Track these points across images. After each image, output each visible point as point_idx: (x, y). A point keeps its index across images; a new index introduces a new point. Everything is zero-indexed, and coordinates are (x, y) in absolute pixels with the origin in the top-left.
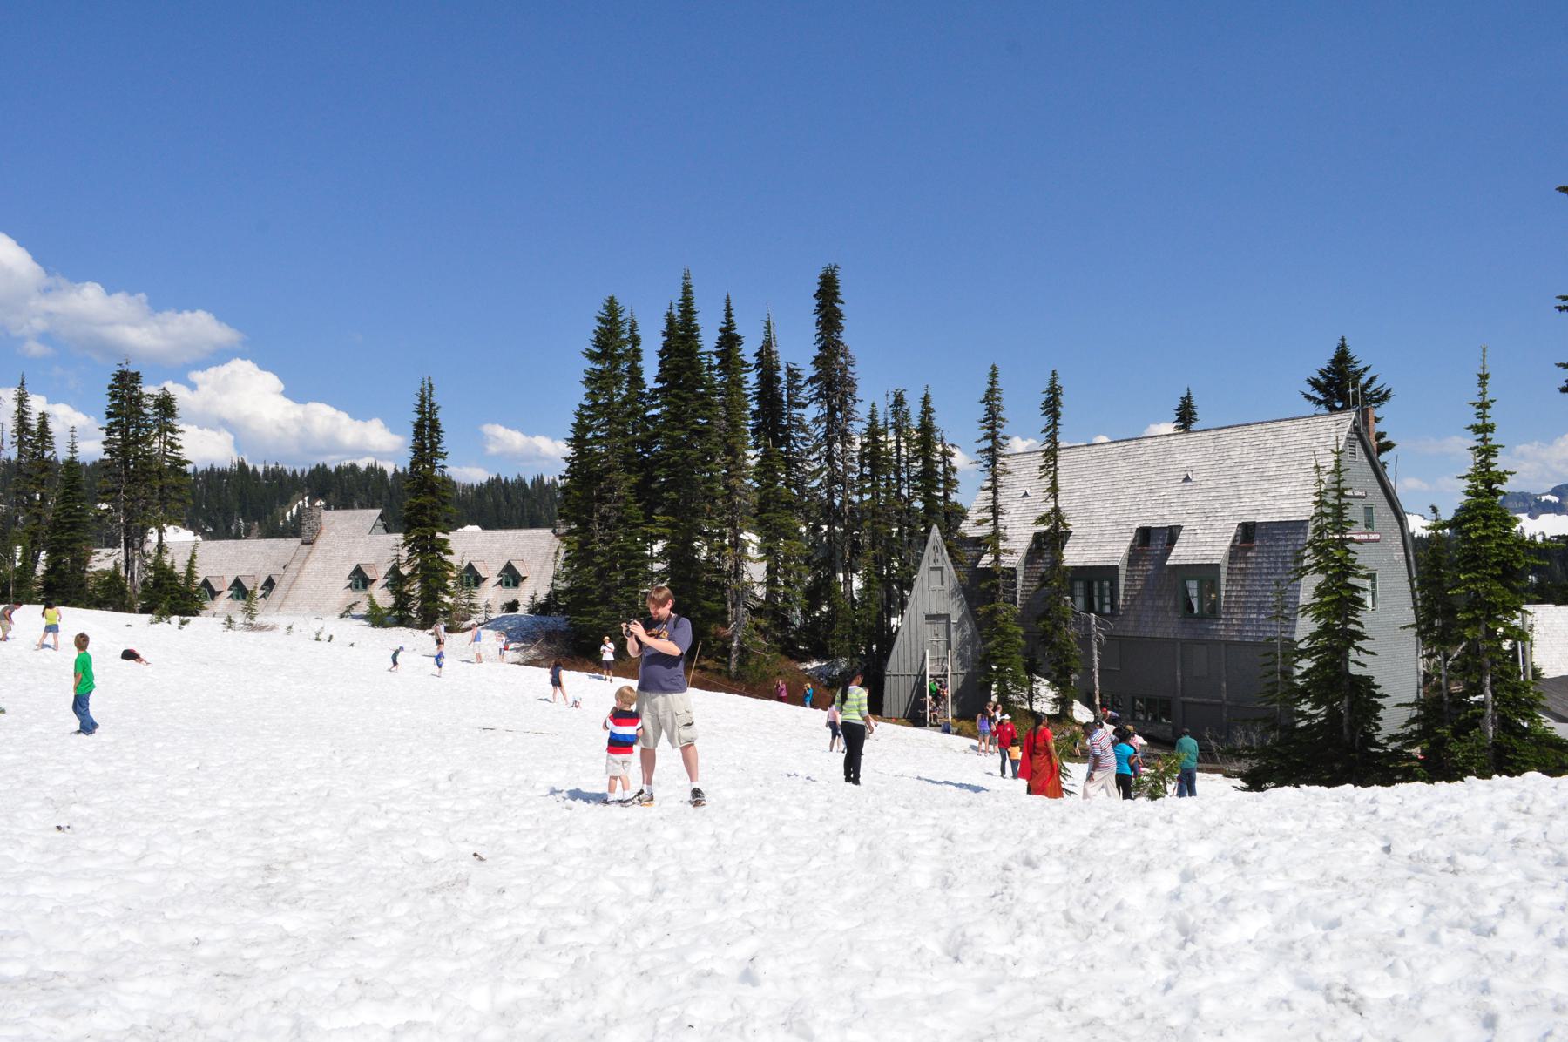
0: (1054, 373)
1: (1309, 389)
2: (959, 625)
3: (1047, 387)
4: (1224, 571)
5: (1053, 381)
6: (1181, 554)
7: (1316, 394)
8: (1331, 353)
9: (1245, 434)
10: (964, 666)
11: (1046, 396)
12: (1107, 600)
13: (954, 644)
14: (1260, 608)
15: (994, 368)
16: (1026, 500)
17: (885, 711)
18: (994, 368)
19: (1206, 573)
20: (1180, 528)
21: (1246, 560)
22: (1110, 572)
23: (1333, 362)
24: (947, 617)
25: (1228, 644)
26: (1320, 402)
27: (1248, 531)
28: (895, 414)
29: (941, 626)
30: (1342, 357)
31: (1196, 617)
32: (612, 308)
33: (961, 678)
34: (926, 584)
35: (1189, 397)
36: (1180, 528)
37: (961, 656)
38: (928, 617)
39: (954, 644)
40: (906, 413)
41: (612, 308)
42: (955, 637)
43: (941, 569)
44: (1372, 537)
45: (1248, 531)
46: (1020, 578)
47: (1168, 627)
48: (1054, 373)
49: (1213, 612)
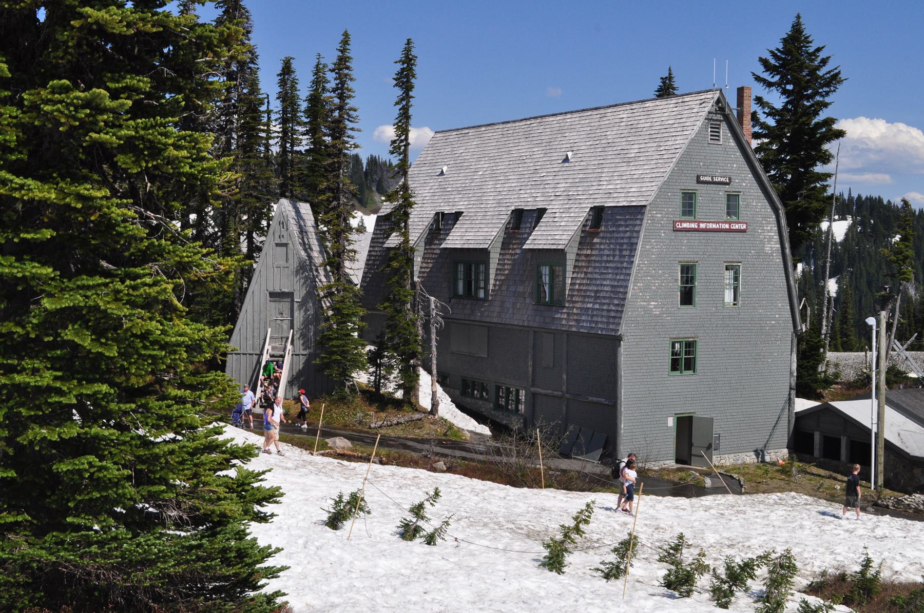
0: (409, 42)
1: (760, 70)
2: (303, 304)
3: (399, 56)
4: (571, 258)
5: (407, 51)
6: (539, 238)
7: (767, 76)
8: (786, 30)
9: (623, 113)
10: (306, 346)
11: (399, 67)
12: (482, 284)
13: (297, 324)
14: (596, 298)
15: (346, 35)
16: (441, 179)
17: (644, 424)
18: (346, 35)
19: (555, 256)
20: (545, 210)
21: (592, 246)
22: (482, 255)
23: (785, 41)
24: (290, 295)
25: (570, 334)
26: (770, 85)
27: (598, 213)
28: (283, 83)
29: (285, 306)
30: (796, 39)
31: (546, 304)
32: (797, 29)
33: (302, 359)
34: (270, 261)
35: (670, 78)
36: (545, 210)
37: (303, 336)
38: (273, 295)
39: (297, 324)
40: (294, 82)
41: (797, 29)
42: (299, 316)
43: (286, 245)
44: (736, 227)
45: (598, 213)
46: (418, 259)
47: (521, 314)
48: (409, 42)
49: (557, 303)
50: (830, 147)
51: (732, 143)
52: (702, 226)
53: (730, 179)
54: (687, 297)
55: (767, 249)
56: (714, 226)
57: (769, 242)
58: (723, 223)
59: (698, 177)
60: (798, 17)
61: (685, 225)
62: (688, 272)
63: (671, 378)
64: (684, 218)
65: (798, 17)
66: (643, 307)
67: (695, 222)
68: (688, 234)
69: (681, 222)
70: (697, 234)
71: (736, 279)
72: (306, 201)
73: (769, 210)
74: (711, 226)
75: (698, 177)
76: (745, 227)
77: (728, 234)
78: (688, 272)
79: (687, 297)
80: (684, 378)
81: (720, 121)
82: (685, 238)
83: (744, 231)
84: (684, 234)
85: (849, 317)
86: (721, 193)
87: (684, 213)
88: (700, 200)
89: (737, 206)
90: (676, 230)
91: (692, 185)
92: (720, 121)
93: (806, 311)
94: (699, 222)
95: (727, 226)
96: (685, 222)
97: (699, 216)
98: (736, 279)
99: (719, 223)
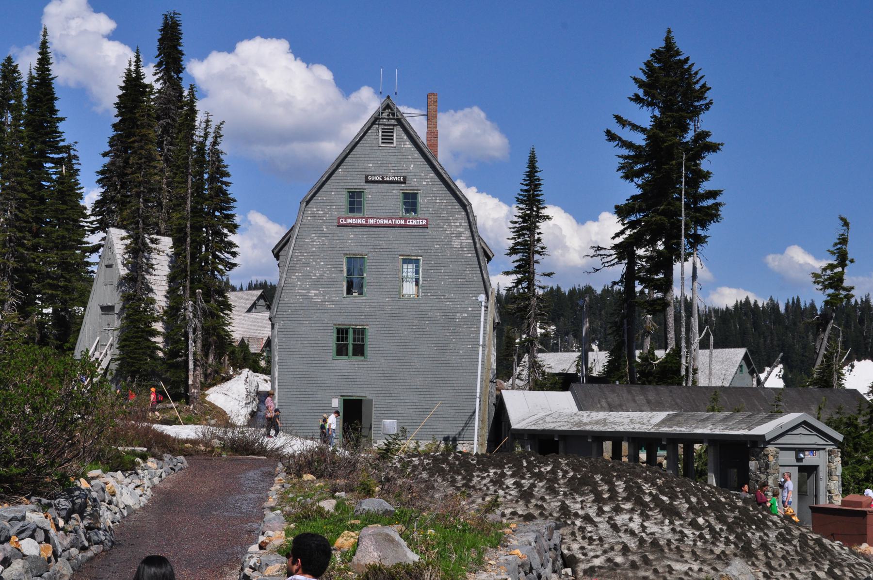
50: (117, 100)
51: (409, 145)
52: (371, 222)
53: (405, 178)
55: (456, 244)
56: (386, 222)
59: (366, 177)
60: (669, 32)
61: (350, 221)
63: (336, 362)
64: (351, 215)
65: (669, 32)
66: (304, 295)
67: (362, 218)
68: (355, 229)
69: (346, 218)
70: (366, 229)
71: (417, 272)
72: (168, 236)
73: (457, 206)
74: (381, 222)
75: (366, 177)
76: (424, 222)
77: (404, 230)
80: (349, 364)
81: (394, 125)
82: (351, 234)
83: (424, 227)
86: (397, 191)
87: (352, 210)
88: (368, 197)
91: (358, 184)
92: (394, 125)
93: (709, 340)
95: (402, 222)
96: (350, 218)
97: (366, 213)
98: (417, 272)
99: (392, 219)
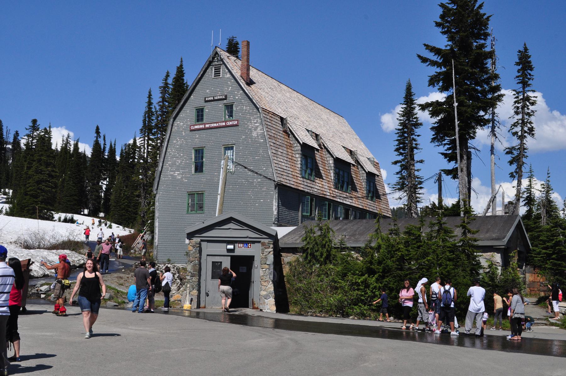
35: (526, 49)
52: (207, 126)
54: (199, 168)
56: (215, 125)
57: (255, 130)
58: (221, 122)
60: (525, 44)
61: (196, 127)
62: (199, 153)
74: (213, 125)
76: (236, 122)
78: (199, 153)
79: (199, 168)
82: (197, 135)
83: (236, 125)
84: (196, 132)
85: (299, 166)
86: (221, 105)
88: (206, 110)
89: (202, 115)
90: (191, 131)
94: (205, 124)
95: (224, 124)
99: (218, 123)
